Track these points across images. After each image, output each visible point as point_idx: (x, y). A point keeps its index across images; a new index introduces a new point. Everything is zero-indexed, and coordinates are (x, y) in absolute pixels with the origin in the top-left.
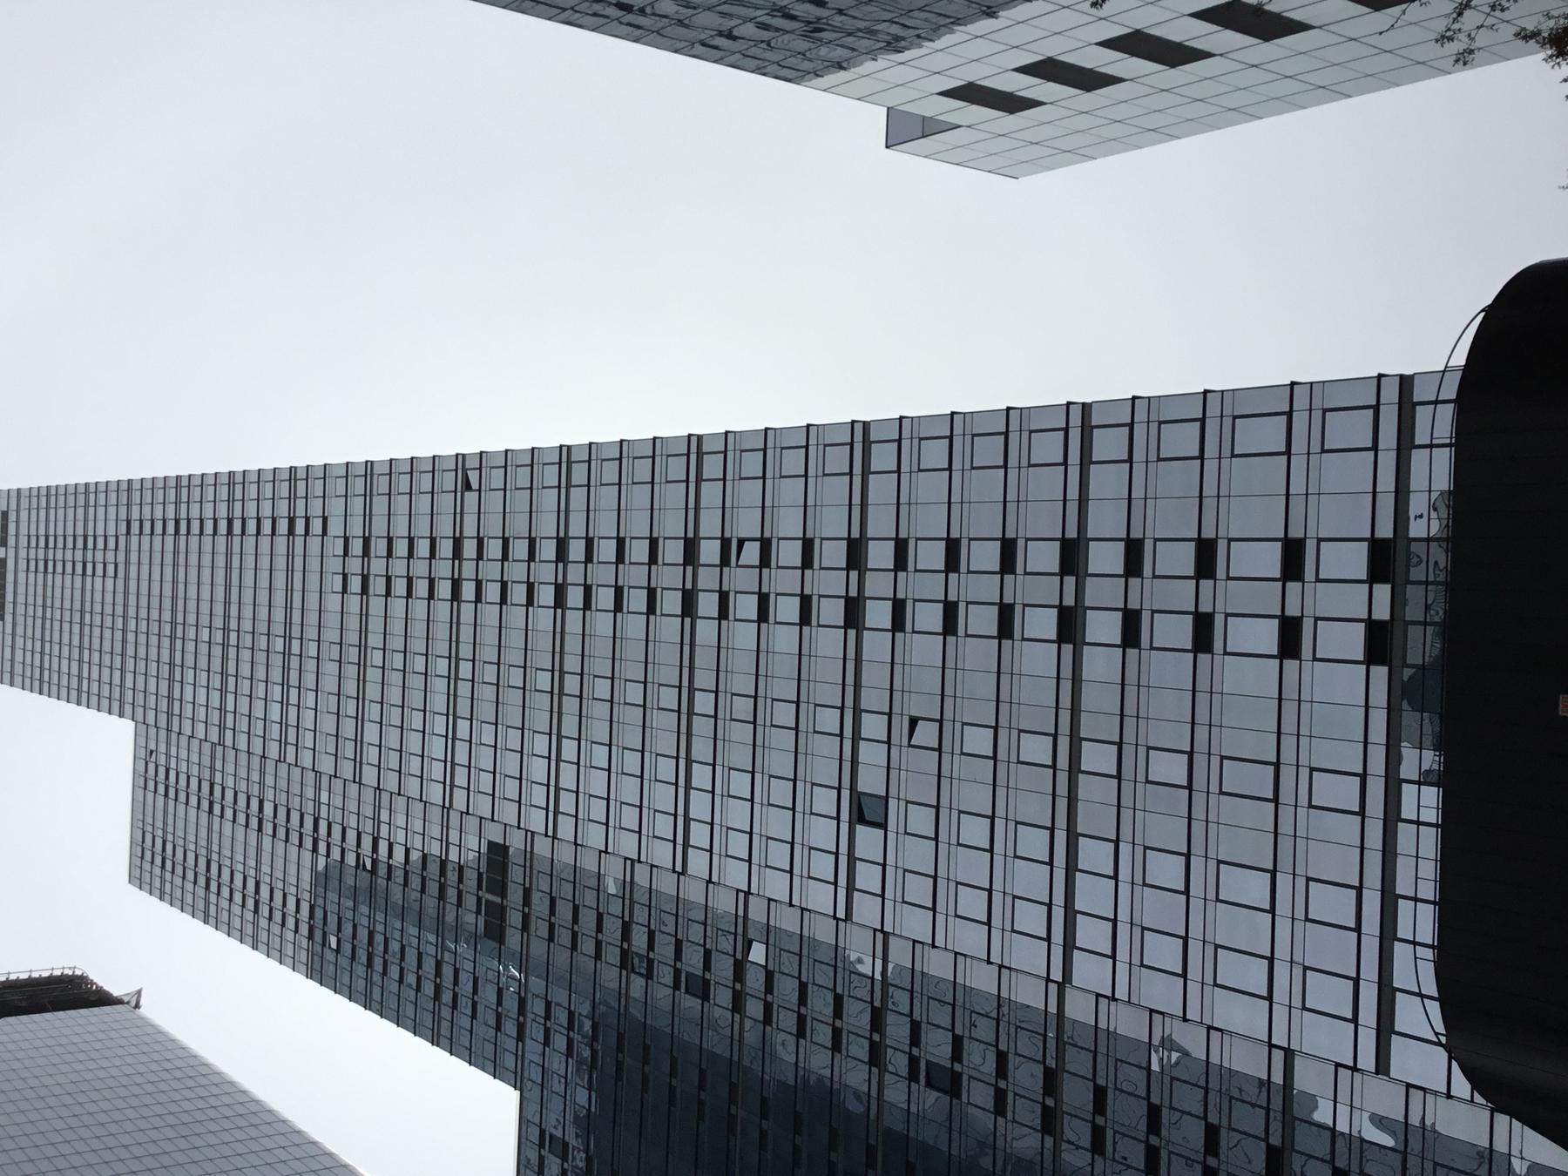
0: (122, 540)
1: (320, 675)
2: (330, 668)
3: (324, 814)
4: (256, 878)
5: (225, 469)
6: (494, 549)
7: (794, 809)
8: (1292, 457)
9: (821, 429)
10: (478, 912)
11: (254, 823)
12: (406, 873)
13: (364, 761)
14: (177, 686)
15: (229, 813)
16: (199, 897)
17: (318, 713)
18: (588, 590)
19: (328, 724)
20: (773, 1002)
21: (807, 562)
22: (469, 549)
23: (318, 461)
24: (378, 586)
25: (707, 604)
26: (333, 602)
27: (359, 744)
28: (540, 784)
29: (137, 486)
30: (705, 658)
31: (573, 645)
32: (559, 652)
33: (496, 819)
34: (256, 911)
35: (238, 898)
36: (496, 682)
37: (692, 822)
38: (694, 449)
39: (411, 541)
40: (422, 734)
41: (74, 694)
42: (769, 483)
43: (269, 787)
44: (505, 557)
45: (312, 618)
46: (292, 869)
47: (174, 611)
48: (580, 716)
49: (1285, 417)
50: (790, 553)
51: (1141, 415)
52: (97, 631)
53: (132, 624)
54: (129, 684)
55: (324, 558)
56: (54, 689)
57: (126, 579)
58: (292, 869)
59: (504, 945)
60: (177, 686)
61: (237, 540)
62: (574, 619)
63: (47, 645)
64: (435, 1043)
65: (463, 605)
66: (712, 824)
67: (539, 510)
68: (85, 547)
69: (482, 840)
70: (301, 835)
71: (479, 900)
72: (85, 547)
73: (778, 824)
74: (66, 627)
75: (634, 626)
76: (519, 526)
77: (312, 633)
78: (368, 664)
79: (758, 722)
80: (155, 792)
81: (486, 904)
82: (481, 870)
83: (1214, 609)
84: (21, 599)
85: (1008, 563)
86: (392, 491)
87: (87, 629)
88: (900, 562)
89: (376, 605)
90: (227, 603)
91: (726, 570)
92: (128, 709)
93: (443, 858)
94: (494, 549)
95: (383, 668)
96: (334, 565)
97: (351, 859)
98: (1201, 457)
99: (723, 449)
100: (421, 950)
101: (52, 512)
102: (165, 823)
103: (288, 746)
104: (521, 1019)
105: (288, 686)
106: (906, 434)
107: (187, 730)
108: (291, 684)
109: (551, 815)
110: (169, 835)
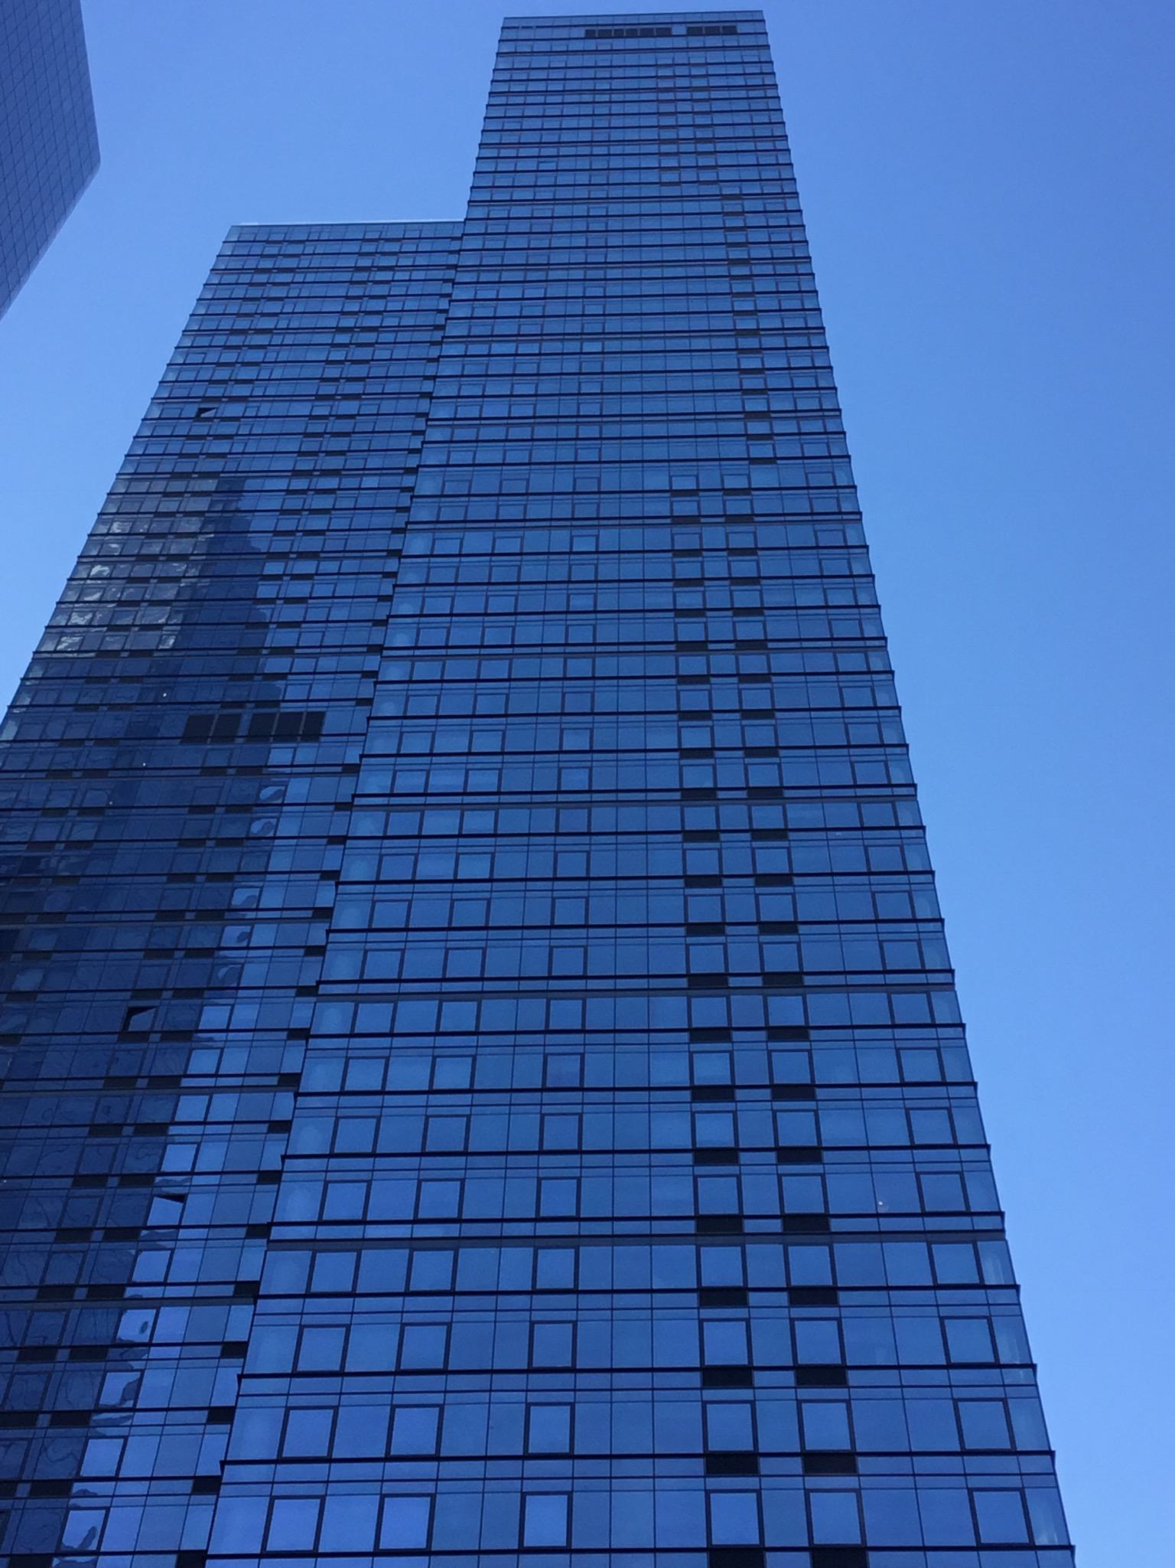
0: (713, 190)
2: (564, 481)
3: (348, 482)
5: (827, 320)
6: (756, 697)
7: (423, 1154)
8: (975, 1553)
9: (922, 841)
11: (328, 389)
12: (250, 677)
14: (518, 276)
15: (338, 355)
16: (245, 262)
18: (711, 835)
19: (485, 482)
20: (195, 883)
21: (788, 1155)
22: (753, 663)
23: (854, 445)
24: (686, 539)
25: (709, 1011)
26: (657, 480)
28: (408, 916)
29: (791, 204)
30: (631, 1011)
31: (631, 818)
32: (618, 797)
33: (372, 722)
35: (222, 374)
36: (545, 1148)
38: (982, 1223)
39: (758, 611)
40: (433, 1030)
41: (494, 138)
42: (905, 1155)
43: (379, 405)
44: (747, 714)
45: (631, 451)
46: (267, 445)
48: (529, 835)
49: (1027, 1541)
50: (797, 1129)
51: (1030, 1464)
52: (588, 109)
53: (597, 210)
54: (517, 211)
55: (709, 353)
56: (499, 112)
57: (661, 198)
58: (267, 445)
60: (518, 276)
61: (730, 343)
62: (667, 817)
63: (558, 99)
64: (37, 656)
65: (671, 659)
66: (353, 1294)
67: (896, 1311)
68: (697, 140)
69: (325, 704)
70: (315, 454)
71: (240, 704)
72: (697, 140)
73: (400, 1133)
74: (586, 122)
75: (668, 905)
76: (794, 731)
77: (610, 452)
78: (575, 532)
79: (554, 931)
80: (360, 254)
82: (283, 705)
83: (739, 1101)
84: (617, 59)
85: (812, 1375)
86: (804, 437)
87: (586, 150)
88: (803, 1296)
89: (660, 538)
90: (641, 335)
91: (772, 1157)
92: (479, 212)
93: (185, 1082)
94: (756, 697)
95: (571, 553)
96: (710, 477)
97: (265, 590)
98: (950, 1366)
99: (893, 782)
100: (236, 438)
101: (743, 94)
103: (449, 430)
106: (966, 1154)
107: (459, 293)
110: (303, 275)
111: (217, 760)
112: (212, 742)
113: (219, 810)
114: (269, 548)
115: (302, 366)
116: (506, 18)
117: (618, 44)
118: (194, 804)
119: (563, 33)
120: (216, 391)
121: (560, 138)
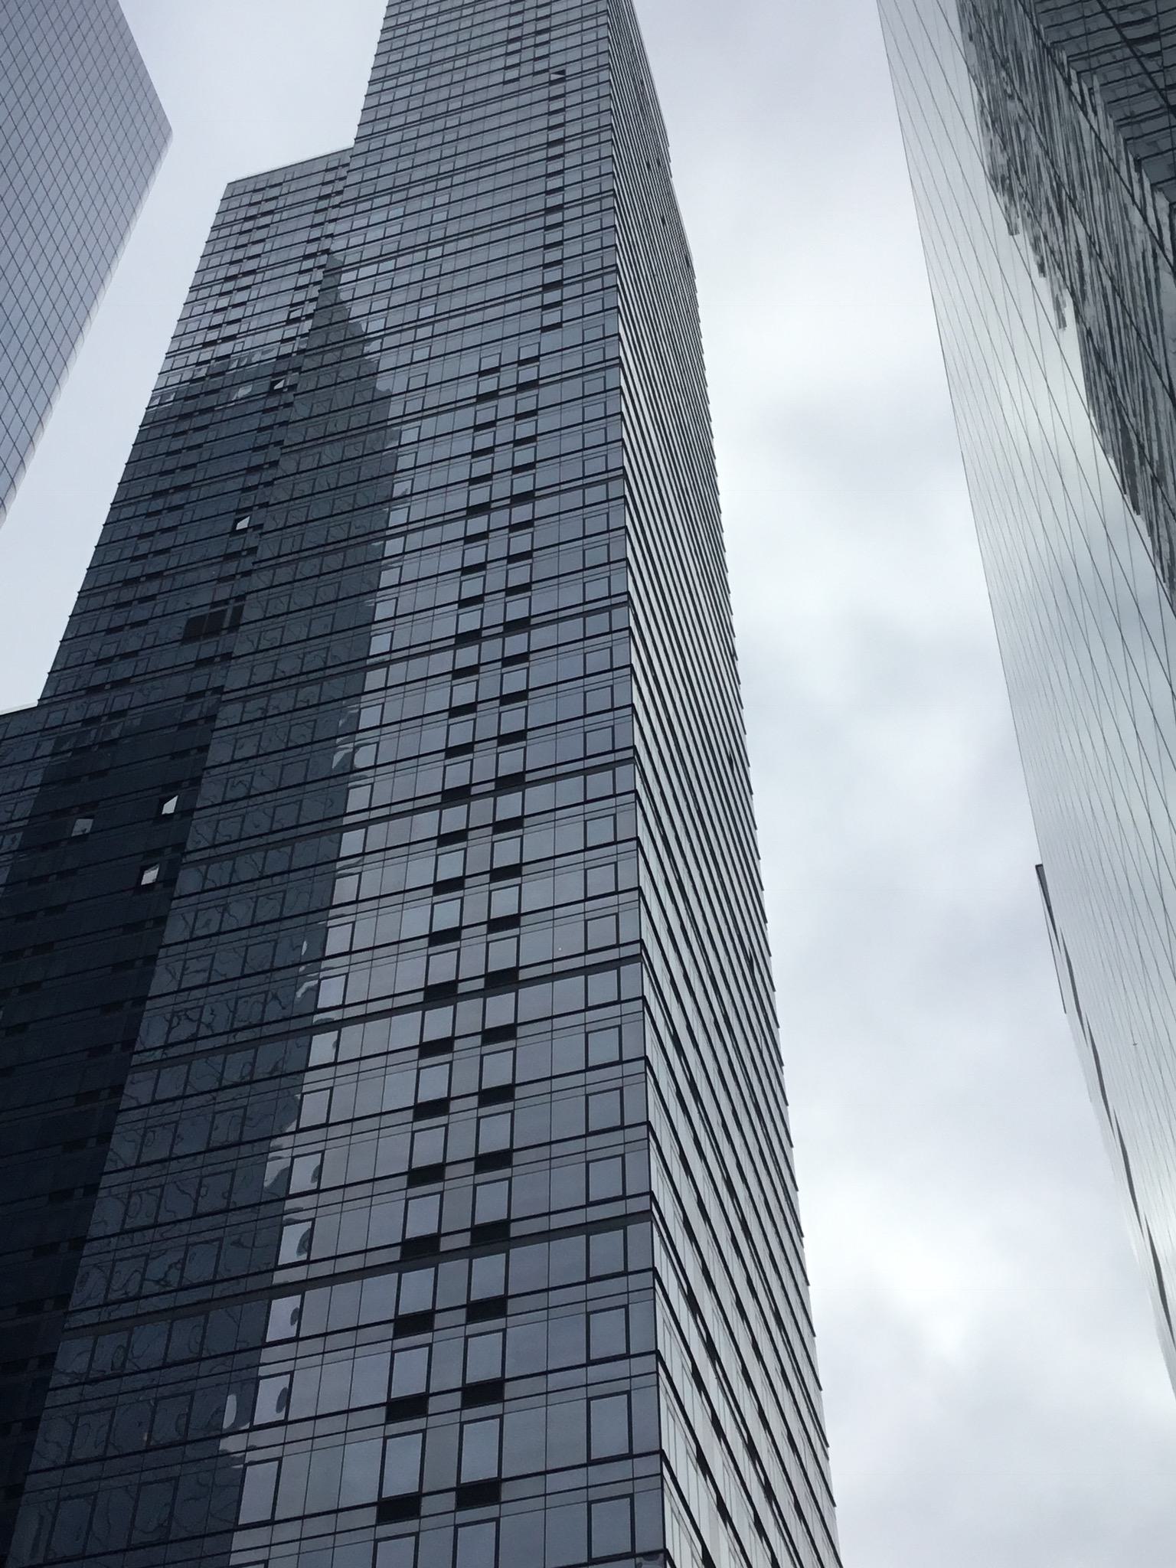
1: (500, 342)
4: (239, 333)
10: (214, 604)
13: (586, 378)
17: (580, 320)
27: (603, 365)
34: (205, 345)
37: (611, 772)
45: (454, 343)
47: (466, 169)
59: (182, 644)
77: (438, 347)
81: (223, 610)
90: (471, 233)
102: (292, 206)
105: (601, 276)
108: (605, 277)
109: (580, 609)
112: (205, 639)
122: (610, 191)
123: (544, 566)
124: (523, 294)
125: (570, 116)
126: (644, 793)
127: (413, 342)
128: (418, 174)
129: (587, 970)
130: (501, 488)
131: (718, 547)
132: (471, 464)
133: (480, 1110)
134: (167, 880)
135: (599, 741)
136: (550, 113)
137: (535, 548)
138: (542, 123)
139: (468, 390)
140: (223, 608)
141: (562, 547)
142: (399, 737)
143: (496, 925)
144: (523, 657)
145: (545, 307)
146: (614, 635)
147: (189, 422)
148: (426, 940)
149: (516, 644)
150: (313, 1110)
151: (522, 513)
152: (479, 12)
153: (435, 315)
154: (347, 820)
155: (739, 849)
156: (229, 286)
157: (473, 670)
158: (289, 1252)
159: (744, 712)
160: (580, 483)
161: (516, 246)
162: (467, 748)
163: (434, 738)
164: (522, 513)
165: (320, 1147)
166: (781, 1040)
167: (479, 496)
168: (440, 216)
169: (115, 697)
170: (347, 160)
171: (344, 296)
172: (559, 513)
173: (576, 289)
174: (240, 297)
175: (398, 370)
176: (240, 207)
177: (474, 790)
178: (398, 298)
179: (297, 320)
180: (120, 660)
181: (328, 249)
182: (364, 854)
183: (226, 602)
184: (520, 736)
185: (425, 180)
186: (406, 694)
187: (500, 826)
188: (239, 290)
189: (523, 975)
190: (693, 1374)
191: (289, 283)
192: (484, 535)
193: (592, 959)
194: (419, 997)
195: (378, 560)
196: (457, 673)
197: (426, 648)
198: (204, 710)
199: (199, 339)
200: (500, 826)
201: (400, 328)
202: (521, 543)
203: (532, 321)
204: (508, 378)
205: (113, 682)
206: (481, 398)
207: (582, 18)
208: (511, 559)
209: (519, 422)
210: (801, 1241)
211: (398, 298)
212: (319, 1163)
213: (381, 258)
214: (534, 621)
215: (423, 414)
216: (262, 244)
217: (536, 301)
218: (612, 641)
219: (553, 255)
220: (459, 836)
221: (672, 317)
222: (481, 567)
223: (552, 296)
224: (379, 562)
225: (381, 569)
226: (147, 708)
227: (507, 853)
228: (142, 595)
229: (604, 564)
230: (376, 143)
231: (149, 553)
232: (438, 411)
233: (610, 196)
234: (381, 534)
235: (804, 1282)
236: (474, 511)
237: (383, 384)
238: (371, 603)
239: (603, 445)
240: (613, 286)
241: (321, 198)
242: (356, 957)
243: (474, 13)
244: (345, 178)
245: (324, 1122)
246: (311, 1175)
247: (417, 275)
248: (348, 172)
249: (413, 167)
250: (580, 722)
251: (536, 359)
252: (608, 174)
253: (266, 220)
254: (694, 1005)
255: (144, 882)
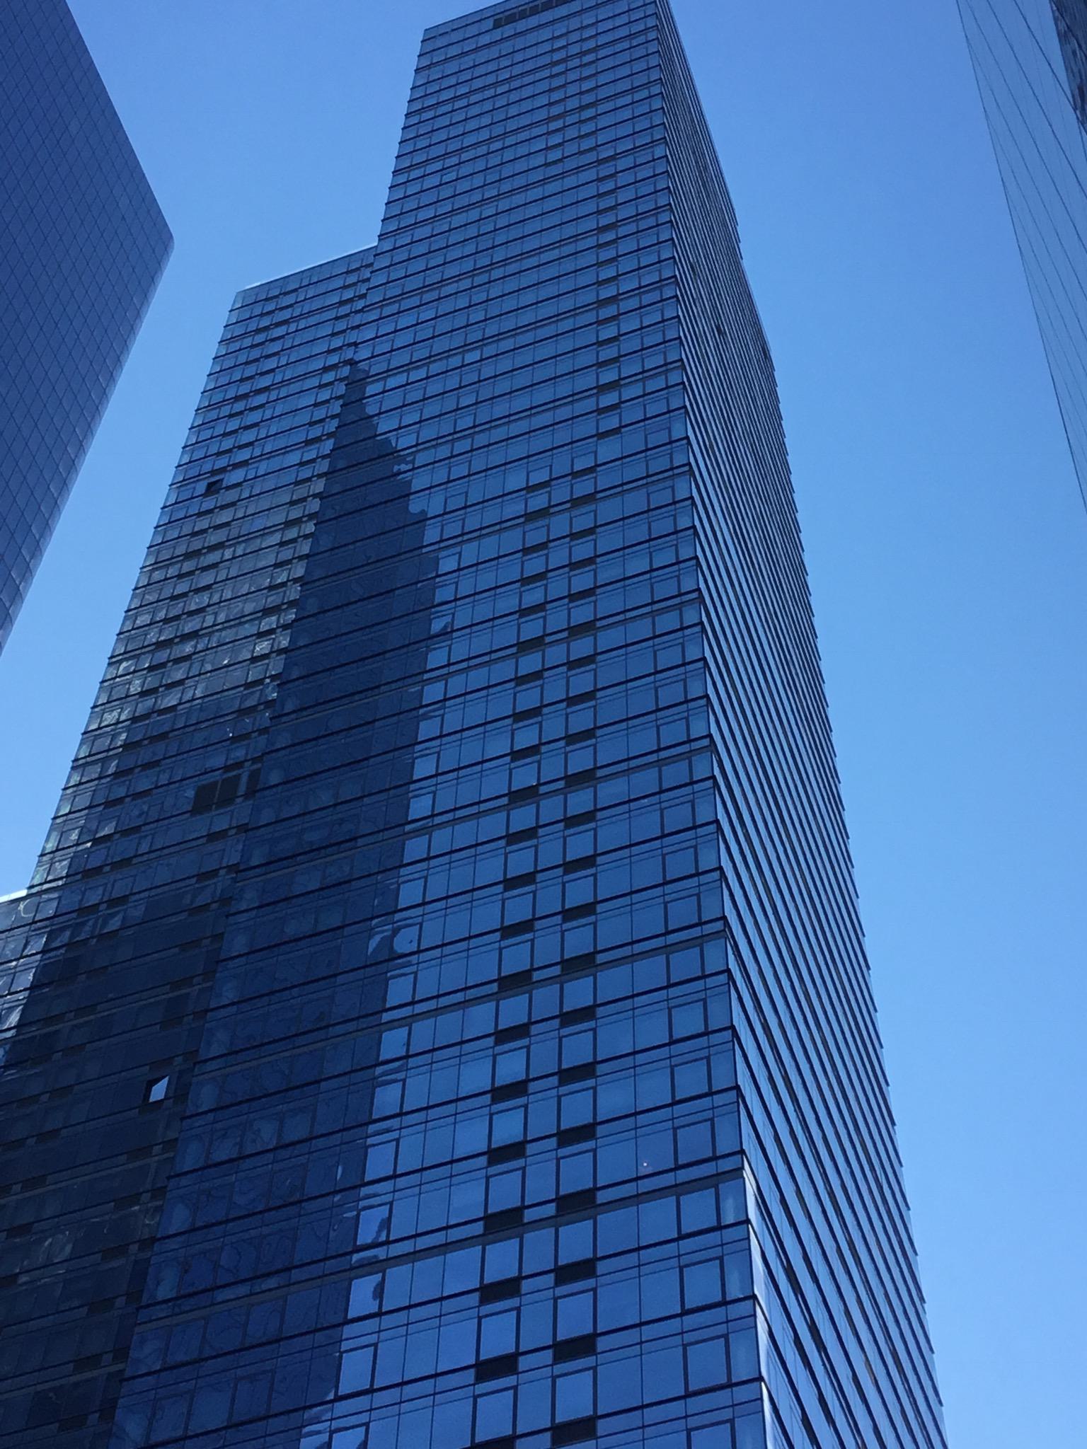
10: (227, 768)
13: (652, 489)
28: (536, 860)
64: (76, 764)
90: (515, 332)
104: (107, 869)
111: (221, 824)
112: (217, 809)
113: (222, 872)
114: (598, 429)
115: (560, 263)
116: (426, 30)
117: (521, 25)
118: (203, 870)
119: (473, 30)
120: (222, 462)
121: (646, 25)
122: (684, 465)
123: (610, 709)
124: (574, 397)
125: (622, 196)
126: (738, 972)
127: (449, 458)
128: (451, 271)
129: (678, 1190)
130: (557, 619)
131: (816, 678)
132: (515, 695)
133: (565, 877)
134: (179, 1093)
135: (683, 913)
136: (600, 195)
137: (599, 948)
138: (591, 207)
139: (515, 508)
140: (234, 773)
141: (639, 1001)
142: (461, 745)
143: (567, 1137)
144: (589, 817)
145: (600, 411)
146: (699, 830)
147: (245, 402)
148: (476, 1295)
149: (580, 801)
150: (354, 1372)
151: (582, 647)
152: (515, 89)
153: (474, 427)
154: (386, 1017)
155: (817, 739)
156: (239, 406)
157: (530, 833)
158: (366, 1234)
159: (855, 872)
160: (653, 758)
161: (566, 344)
162: (525, 927)
163: (488, 915)
164: (582, 647)
165: (364, 1418)
166: (892, 1100)
167: (531, 629)
168: (478, 315)
169: (115, 881)
170: (371, 259)
171: (371, 410)
172: (627, 646)
173: (636, 390)
174: (254, 417)
175: (436, 465)
176: (251, 318)
177: (537, 976)
178: (431, 409)
179: (317, 440)
180: (173, 665)
181: (352, 359)
182: (407, 1057)
183: (239, 765)
184: (588, 909)
185: (459, 277)
186: (460, 780)
187: (568, 1018)
188: (252, 409)
189: (602, 1197)
190: (802, 1420)
191: (309, 400)
192: (537, 675)
193: (683, 1176)
194: (478, 1228)
195: (414, 709)
196: (513, 838)
197: (474, 809)
198: (218, 892)
199: (181, 550)
200: (568, 1018)
201: (436, 442)
202: (582, 682)
203: (586, 427)
204: (561, 493)
205: (112, 863)
206: (530, 517)
207: (633, 88)
208: (571, 701)
209: (573, 672)
210: (923, 1307)
211: (431, 409)
212: (363, 1437)
213: (410, 366)
214: (600, 958)
215: (464, 537)
216: (232, 509)
217: (590, 404)
218: (693, 793)
219: (608, 353)
220: (520, 1031)
221: (750, 416)
222: (535, 712)
223: (609, 399)
224: (416, 711)
225: (375, 1083)
226: (153, 892)
227: (578, 1050)
228: (145, 761)
229: (681, 703)
230: (422, 143)
231: (169, 661)
232: (481, 533)
233: (667, 210)
234: (418, 678)
235: (937, 1402)
236: (525, 647)
237: (415, 506)
238: (392, 884)
239: (681, 703)
240: (684, 465)
241: (342, 303)
242: (401, 1182)
243: (510, 91)
244: (368, 280)
245: (398, 1111)
246: (371, 1295)
247: (453, 382)
248: (371, 272)
249: (444, 264)
250: (658, 891)
251: (591, 531)
252: (663, 189)
253: (261, 399)
254: (803, 1168)
255: (152, 1099)
